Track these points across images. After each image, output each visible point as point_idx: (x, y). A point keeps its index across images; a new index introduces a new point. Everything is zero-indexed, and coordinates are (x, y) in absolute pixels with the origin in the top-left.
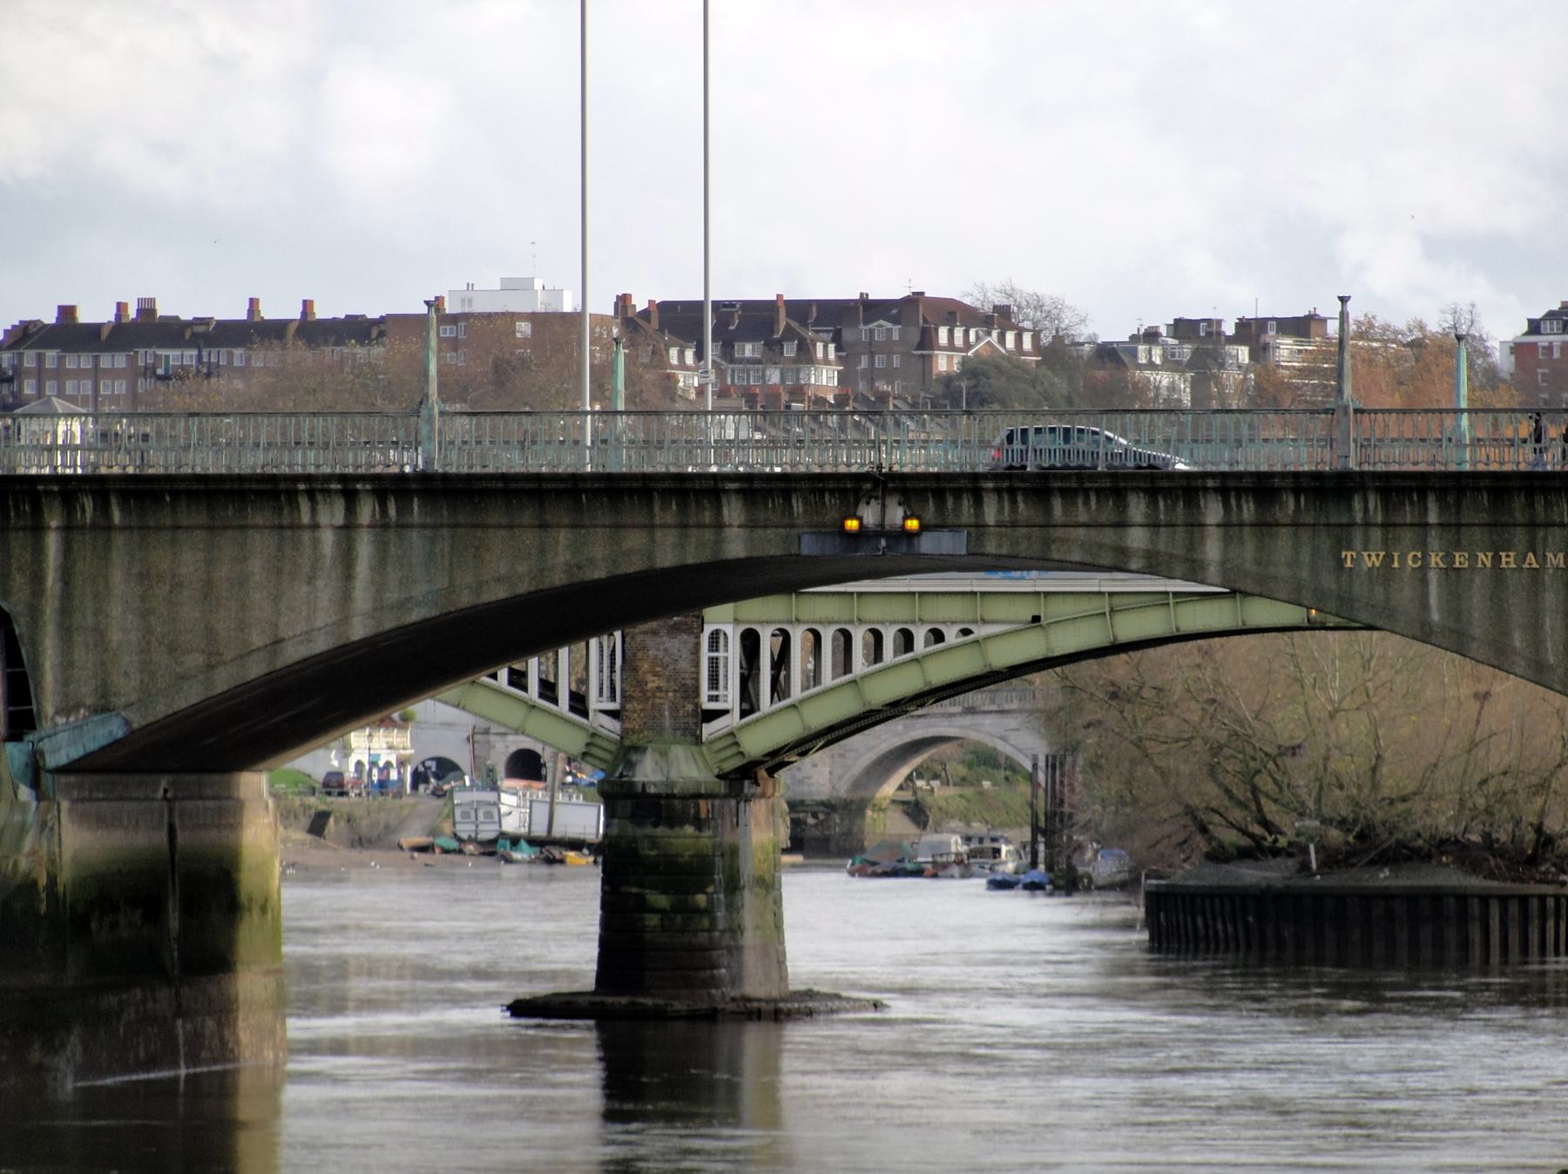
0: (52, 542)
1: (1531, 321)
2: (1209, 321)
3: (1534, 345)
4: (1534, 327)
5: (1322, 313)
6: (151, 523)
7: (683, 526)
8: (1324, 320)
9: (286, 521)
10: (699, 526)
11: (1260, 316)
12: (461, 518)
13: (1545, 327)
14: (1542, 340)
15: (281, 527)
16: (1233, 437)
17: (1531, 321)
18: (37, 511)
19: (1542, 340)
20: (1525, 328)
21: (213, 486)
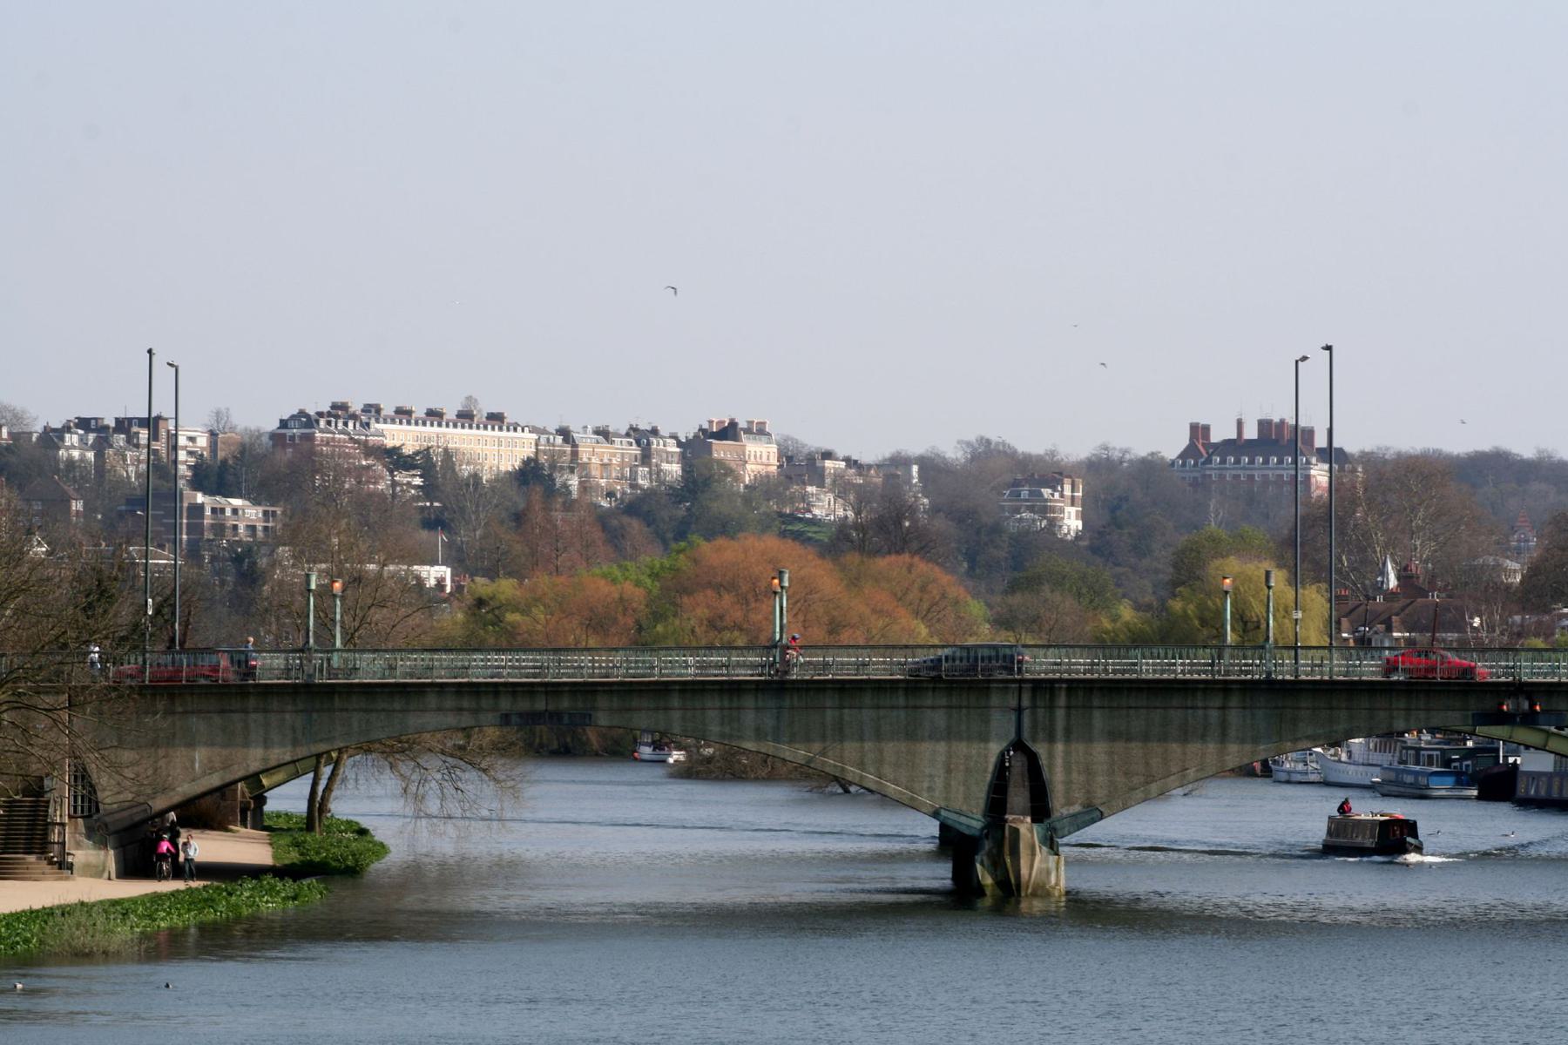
0: (1060, 714)
1: (281, 421)
2: (96, 419)
3: (284, 435)
4: (284, 424)
5: (165, 415)
6: (1200, 704)
7: (1408, 709)
8: (166, 419)
9: (1189, 704)
10: (1417, 709)
11: (129, 416)
12: (955, 701)
13: (291, 424)
14: (288, 432)
15: (1187, 708)
16: (868, 611)
17: (281, 421)
18: (1053, 697)
19: (288, 432)
20: (278, 425)
21: (1318, 687)
